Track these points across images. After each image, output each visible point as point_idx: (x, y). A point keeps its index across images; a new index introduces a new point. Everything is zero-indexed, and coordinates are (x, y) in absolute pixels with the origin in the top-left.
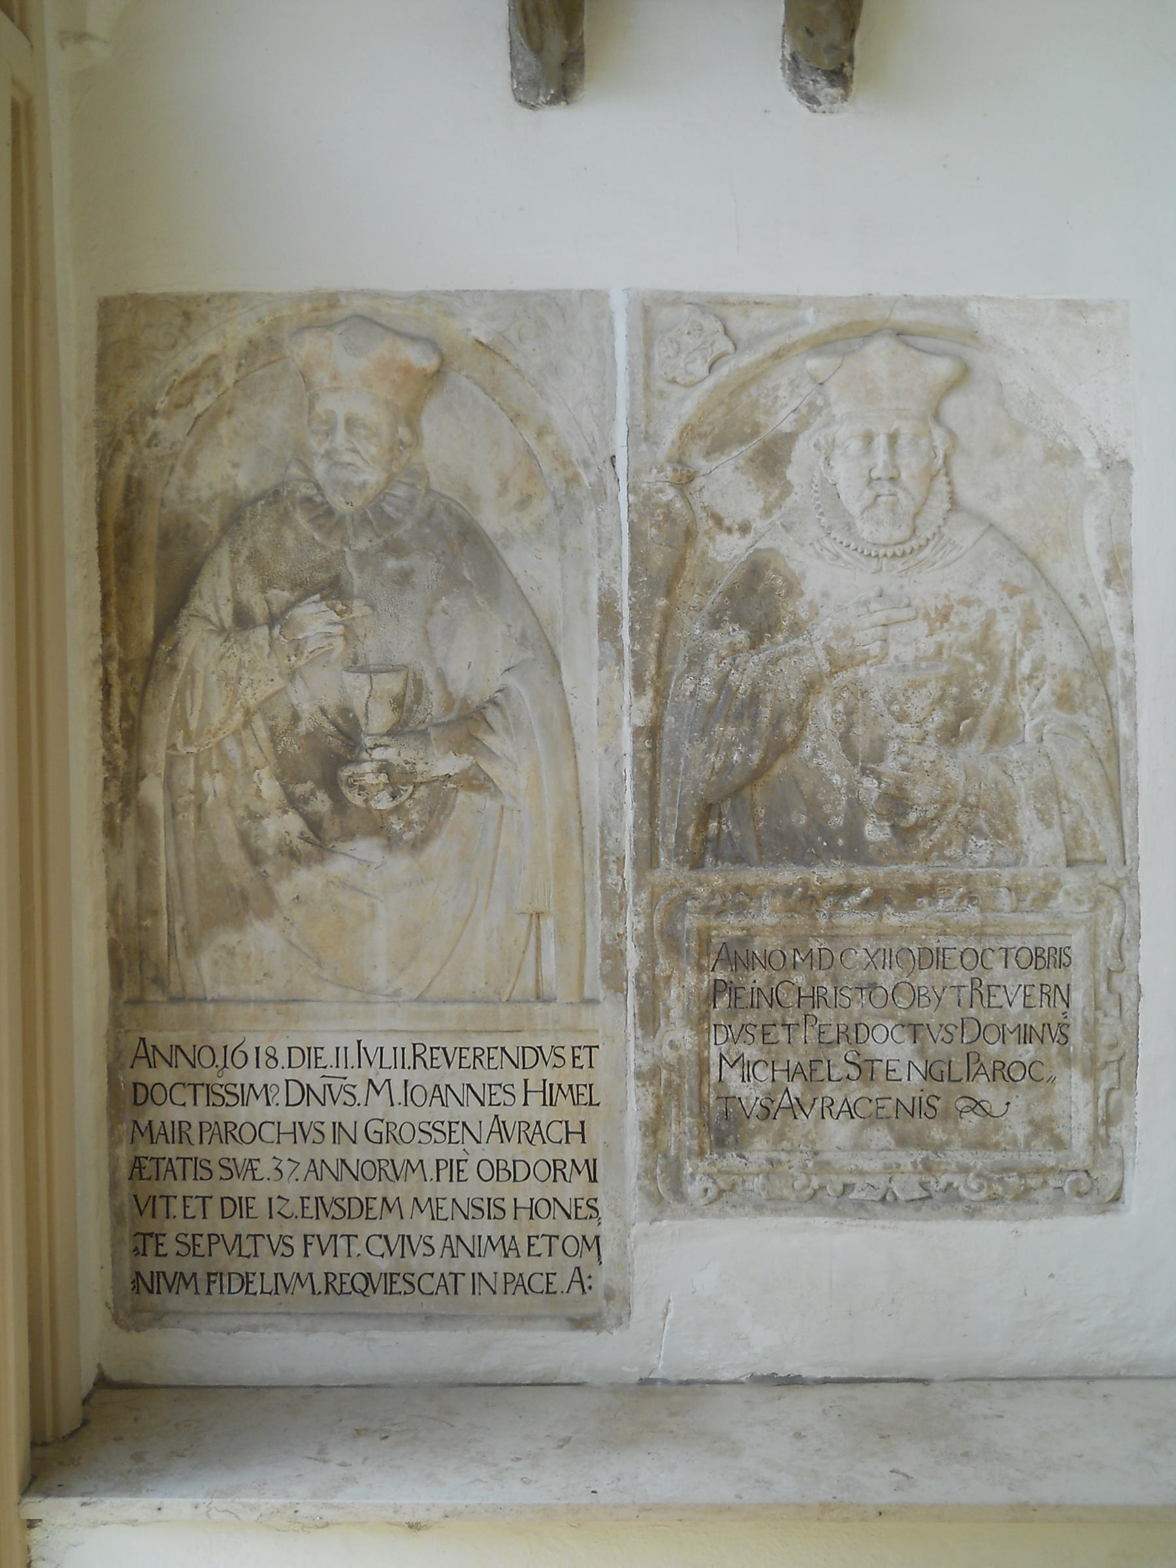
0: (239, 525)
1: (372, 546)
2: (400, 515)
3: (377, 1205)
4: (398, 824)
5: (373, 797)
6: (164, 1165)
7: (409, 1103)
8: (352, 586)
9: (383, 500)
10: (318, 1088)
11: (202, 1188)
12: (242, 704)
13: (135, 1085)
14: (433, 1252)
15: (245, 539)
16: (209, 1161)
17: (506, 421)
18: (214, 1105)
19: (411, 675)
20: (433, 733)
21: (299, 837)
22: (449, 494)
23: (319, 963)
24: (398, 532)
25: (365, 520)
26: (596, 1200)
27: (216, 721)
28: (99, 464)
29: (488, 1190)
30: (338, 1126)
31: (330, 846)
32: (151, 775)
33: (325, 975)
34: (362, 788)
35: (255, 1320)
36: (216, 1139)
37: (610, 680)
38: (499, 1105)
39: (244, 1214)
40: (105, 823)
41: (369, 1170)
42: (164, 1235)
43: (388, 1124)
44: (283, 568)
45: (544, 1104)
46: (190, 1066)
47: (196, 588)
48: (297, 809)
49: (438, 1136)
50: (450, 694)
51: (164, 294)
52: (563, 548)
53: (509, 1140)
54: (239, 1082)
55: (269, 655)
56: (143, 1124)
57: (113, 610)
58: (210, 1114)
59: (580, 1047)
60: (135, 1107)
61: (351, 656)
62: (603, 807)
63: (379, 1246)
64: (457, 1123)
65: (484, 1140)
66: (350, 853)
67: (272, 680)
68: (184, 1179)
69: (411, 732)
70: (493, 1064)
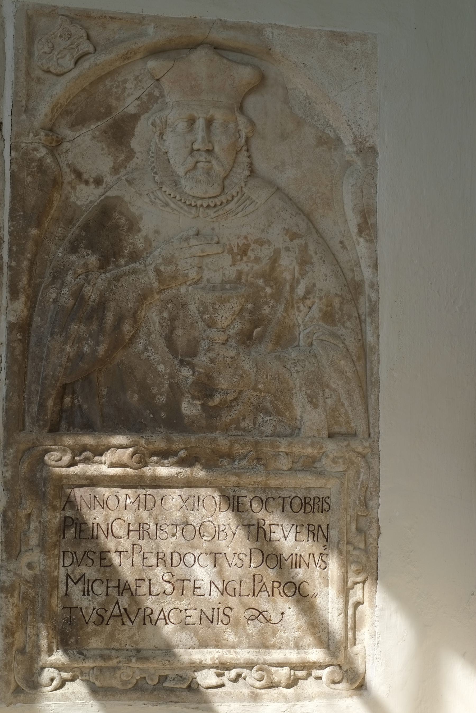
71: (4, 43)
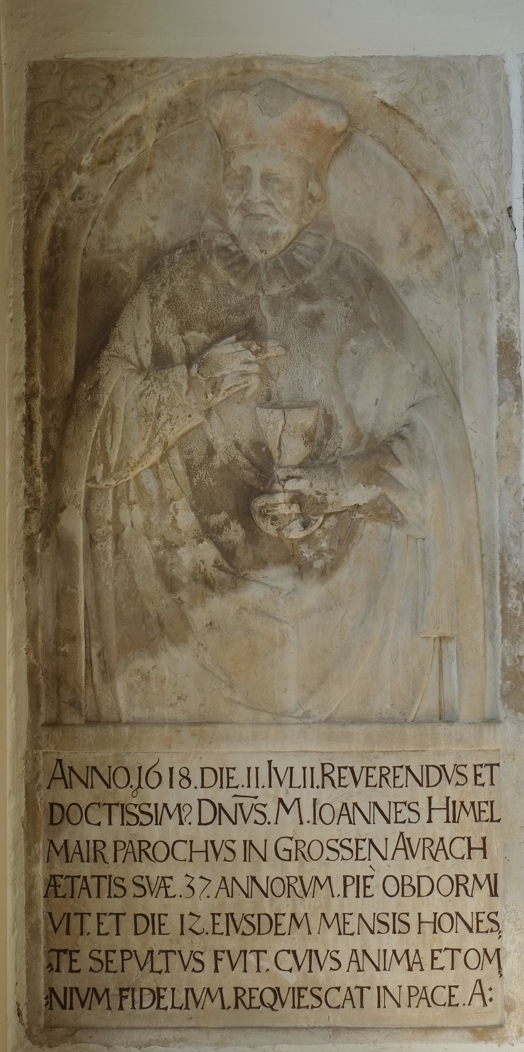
0: (158, 272)
1: (284, 291)
2: (310, 263)
3: (285, 921)
4: (309, 553)
5: (285, 526)
6: (79, 883)
7: (318, 821)
8: (266, 328)
9: (294, 250)
10: (230, 807)
11: (116, 905)
12: (160, 439)
13: (52, 805)
14: (340, 966)
15: (163, 285)
16: (123, 879)
17: (408, 179)
18: (128, 824)
19: (322, 411)
20: (342, 465)
21: (213, 566)
22: (353, 245)
23: (231, 686)
24: (308, 279)
25: (277, 267)
26: (496, 913)
27: (135, 455)
28: (27, 215)
29: (392, 906)
30: (249, 845)
31: (243, 574)
32: (70, 507)
33: (238, 698)
34: (275, 518)
35: (166, 1034)
36: (130, 856)
37: (509, 415)
38: (404, 822)
39: (157, 931)
40: (25, 553)
41: (278, 888)
42: (78, 951)
43: (296, 841)
44: (201, 312)
45: (448, 821)
46: (106, 787)
47: (116, 331)
48: (211, 538)
49: (346, 854)
50: (358, 429)
51: (91, 59)
52: (463, 294)
53: (414, 856)
54: (153, 801)
55: (187, 393)
56: (59, 843)
57: (37, 352)
58: (124, 833)
59: (481, 766)
60: (52, 827)
61: (265, 394)
62: (502, 535)
63: (287, 961)
64: (364, 840)
65: (390, 856)
66: (262, 580)
67: (190, 416)
68: (99, 896)
69: (322, 465)
70: (399, 782)
71: (509, 107)
